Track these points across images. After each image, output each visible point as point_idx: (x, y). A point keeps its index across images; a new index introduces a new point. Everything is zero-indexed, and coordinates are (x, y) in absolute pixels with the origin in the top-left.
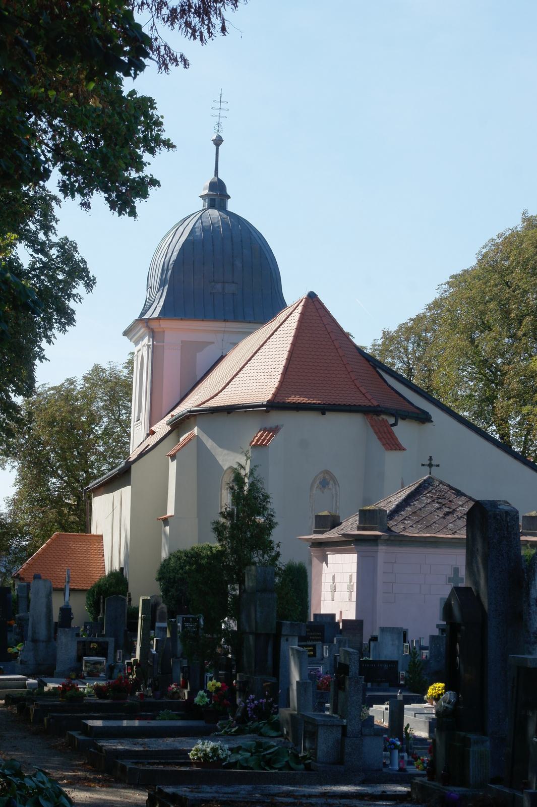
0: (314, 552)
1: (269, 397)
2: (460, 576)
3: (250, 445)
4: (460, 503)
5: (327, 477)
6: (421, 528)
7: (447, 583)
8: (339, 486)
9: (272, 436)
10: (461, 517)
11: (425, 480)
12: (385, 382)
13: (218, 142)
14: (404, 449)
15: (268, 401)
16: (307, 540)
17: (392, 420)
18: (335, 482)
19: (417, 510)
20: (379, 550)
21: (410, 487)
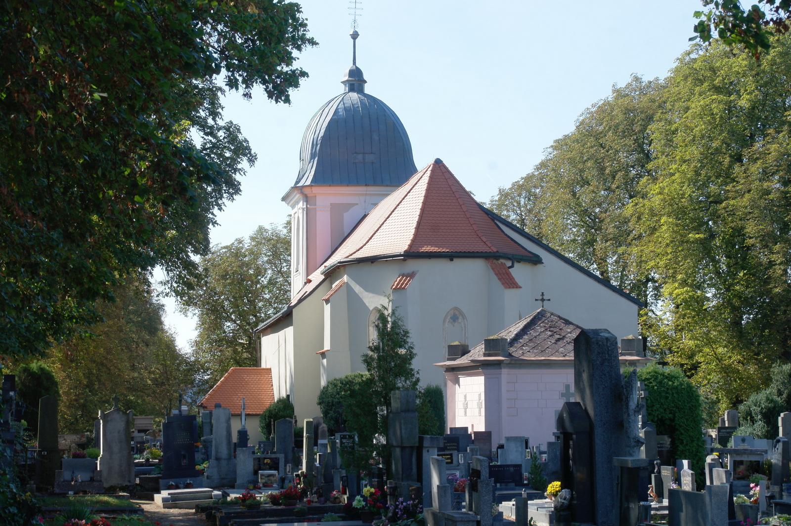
0: (448, 376)
1: (406, 248)
4: (569, 330)
5: (457, 313)
9: (409, 280)
11: (538, 313)
12: (503, 231)
13: (355, 36)
14: (520, 287)
15: (405, 252)
16: (442, 366)
17: (509, 264)
18: (464, 317)
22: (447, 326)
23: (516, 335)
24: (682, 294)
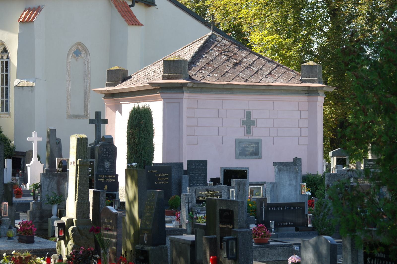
0: (107, 102)
2: (252, 119)
3: (18, 21)
4: (244, 55)
5: (80, 48)
6: (217, 77)
7: (242, 126)
8: (90, 55)
9: (36, 14)
10: (248, 67)
11: (210, 36)
16: (101, 92)
19: (210, 62)
20: (184, 97)
21: (194, 43)
22: (70, 60)
23: (193, 58)
24: (273, 40)
